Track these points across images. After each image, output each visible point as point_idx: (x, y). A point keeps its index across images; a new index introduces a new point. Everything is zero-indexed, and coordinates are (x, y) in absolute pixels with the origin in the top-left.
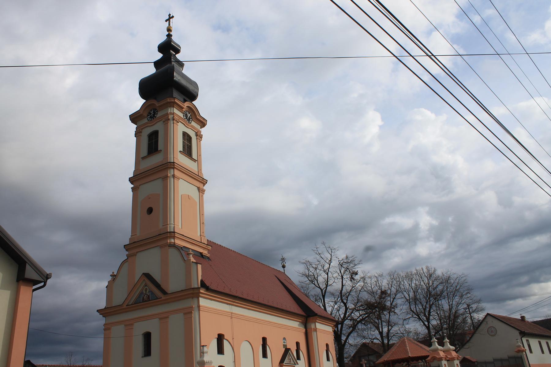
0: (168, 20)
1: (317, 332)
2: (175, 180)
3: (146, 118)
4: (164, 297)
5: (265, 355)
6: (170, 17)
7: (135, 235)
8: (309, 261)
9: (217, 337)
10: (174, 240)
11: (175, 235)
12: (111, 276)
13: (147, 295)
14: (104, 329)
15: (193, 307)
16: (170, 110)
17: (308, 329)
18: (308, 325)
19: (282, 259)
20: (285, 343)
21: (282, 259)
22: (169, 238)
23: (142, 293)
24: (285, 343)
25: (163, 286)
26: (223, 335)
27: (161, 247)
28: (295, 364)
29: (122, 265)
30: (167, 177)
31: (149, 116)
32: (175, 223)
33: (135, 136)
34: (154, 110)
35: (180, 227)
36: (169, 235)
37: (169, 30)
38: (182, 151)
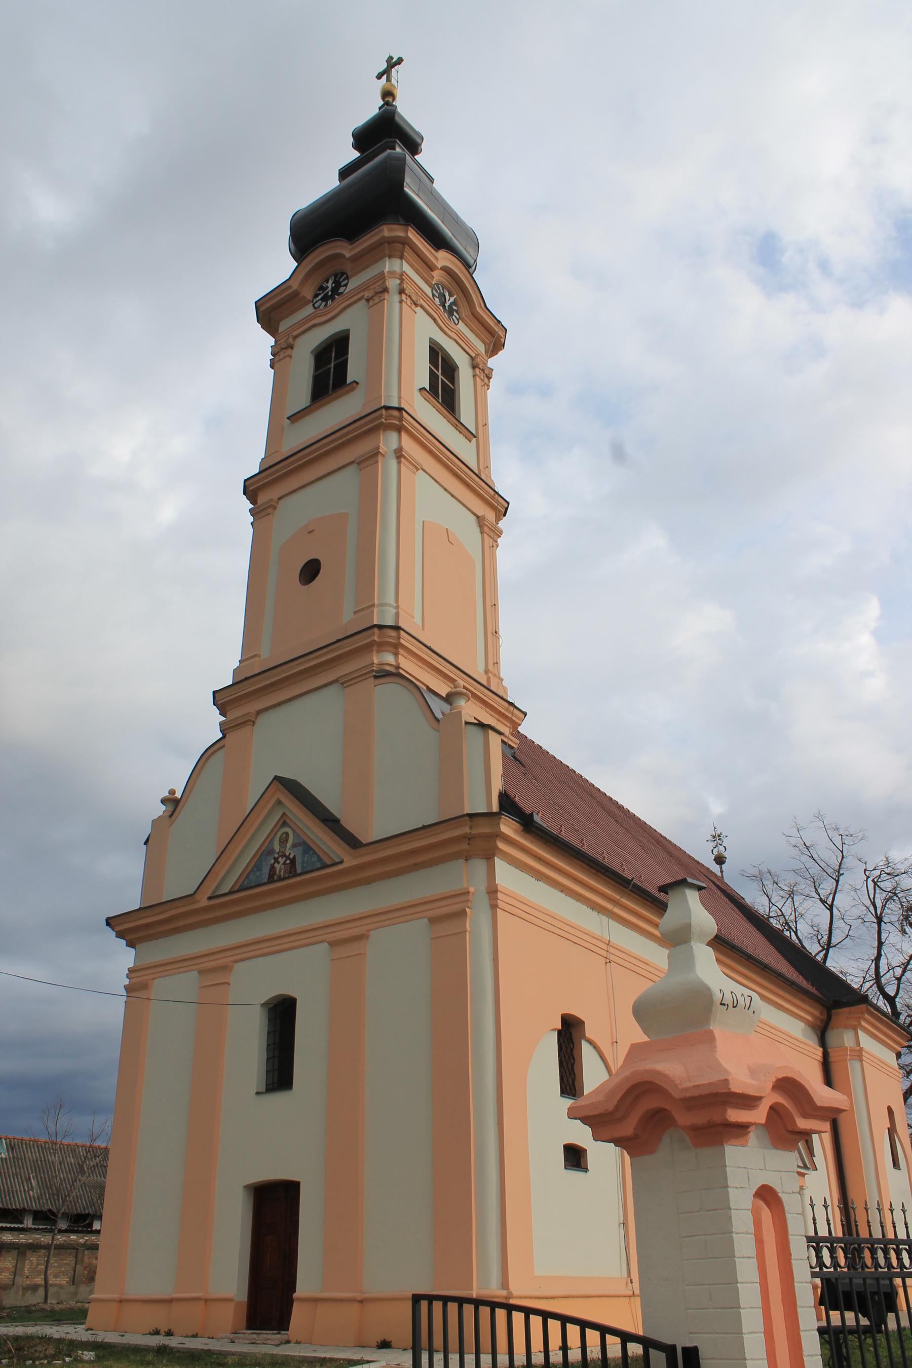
0: (386, 73)
1: (861, 1061)
2: (402, 466)
3: (311, 304)
4: (349, 861)
6: (393, 63)
7: (255, 656)
8: (772, 871)
9: (560, 1027)
10: (397, 659)
11: (399, 638)
12: (164, 801)
13: (288, 857)
14: (125, 986)
15: (468, 893)
16: (390, 265)
17: (829, 1050)
18: (832, 1037)
19: (714, 837)
21: (714, 837)
22: (378, 652)
23: (270, 852)
25: (349, 823)
26: (580, 1023)
27: (344, 682)
28: (805, 1167)
29: (204, 764)
30: (375, 454)
31: (320, 297)
32: (400, 604)
33: (272, 366)
34: (335, 278)
35: (418, 620)
36: (379, 637)
38: (428, 389)
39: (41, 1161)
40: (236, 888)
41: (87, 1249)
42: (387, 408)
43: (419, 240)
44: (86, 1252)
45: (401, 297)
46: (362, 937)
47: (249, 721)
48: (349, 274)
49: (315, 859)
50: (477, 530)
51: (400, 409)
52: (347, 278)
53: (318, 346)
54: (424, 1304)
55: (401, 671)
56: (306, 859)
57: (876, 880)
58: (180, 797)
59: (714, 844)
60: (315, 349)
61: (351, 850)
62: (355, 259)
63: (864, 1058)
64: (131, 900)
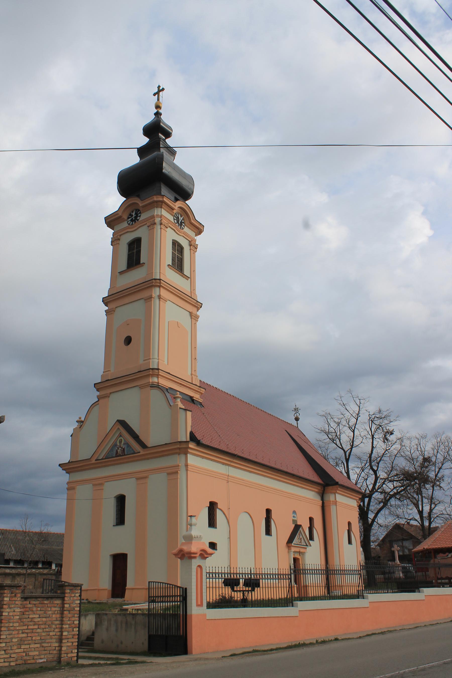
1: (336, 505)
3: (126, 222)
4: (142, 452)
5: (268, 532)
6: (160, 90)
7: (109, 371)
9: (209, 506)
11: (159, 372)
13: (122, 448)
15: (179, 466)
17: (325, 502)
18: (326, 497)
19: (295, 409)
20: (295, 517)
21: (295, 409)
23: (116, 445)
24: (295, 517)
27: (141, 387)
28: (307, 545)
30: (151, 298)
31: (130, 219)
32: (159, 358)
33: (112, 245)
34: (136, 211)
35: (166, 362)
36: (152, 373)
37: (158, 107)
38: (171, 265)
39: (15, 539)
40: (104, 458)
41: (40, 575)
42: (155, 279)
43: (169, 201)
44: (39, 576)
45: (161, 226)
46: (146, 477)
47: (107, 396)
48: (141, 212)
49: (131, 449)
50: (190, 317)
51: (160, 280)
52: (140, 213)
53: (129, 242)
54: (150, 583)
55: (159, 384)
56: (128, 449)
57: (372, 420)
58: (83, 420)
59: (295, 412)
60: (128, 242)
61: (142, 449)
62: (143, 207)
63: (337, 504)
64: (66, 459)
